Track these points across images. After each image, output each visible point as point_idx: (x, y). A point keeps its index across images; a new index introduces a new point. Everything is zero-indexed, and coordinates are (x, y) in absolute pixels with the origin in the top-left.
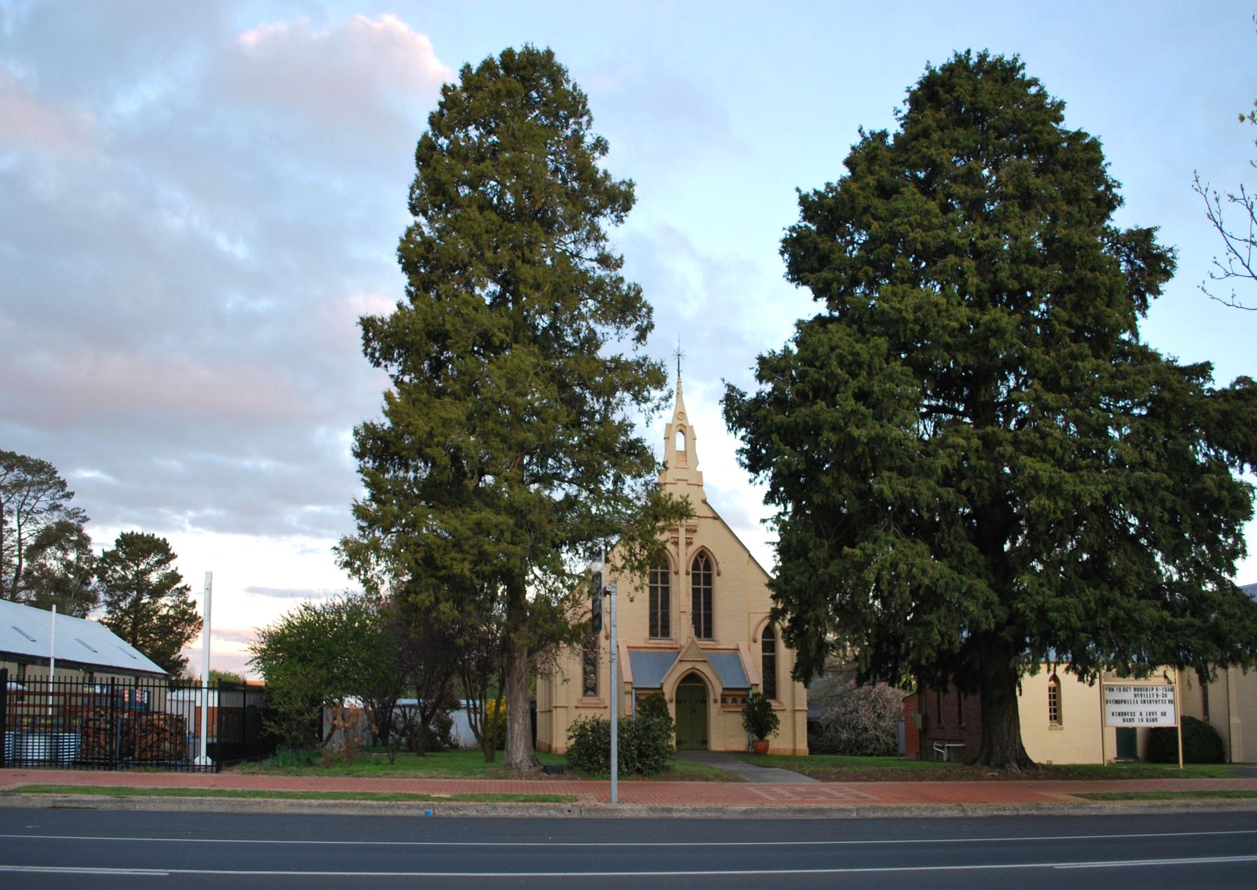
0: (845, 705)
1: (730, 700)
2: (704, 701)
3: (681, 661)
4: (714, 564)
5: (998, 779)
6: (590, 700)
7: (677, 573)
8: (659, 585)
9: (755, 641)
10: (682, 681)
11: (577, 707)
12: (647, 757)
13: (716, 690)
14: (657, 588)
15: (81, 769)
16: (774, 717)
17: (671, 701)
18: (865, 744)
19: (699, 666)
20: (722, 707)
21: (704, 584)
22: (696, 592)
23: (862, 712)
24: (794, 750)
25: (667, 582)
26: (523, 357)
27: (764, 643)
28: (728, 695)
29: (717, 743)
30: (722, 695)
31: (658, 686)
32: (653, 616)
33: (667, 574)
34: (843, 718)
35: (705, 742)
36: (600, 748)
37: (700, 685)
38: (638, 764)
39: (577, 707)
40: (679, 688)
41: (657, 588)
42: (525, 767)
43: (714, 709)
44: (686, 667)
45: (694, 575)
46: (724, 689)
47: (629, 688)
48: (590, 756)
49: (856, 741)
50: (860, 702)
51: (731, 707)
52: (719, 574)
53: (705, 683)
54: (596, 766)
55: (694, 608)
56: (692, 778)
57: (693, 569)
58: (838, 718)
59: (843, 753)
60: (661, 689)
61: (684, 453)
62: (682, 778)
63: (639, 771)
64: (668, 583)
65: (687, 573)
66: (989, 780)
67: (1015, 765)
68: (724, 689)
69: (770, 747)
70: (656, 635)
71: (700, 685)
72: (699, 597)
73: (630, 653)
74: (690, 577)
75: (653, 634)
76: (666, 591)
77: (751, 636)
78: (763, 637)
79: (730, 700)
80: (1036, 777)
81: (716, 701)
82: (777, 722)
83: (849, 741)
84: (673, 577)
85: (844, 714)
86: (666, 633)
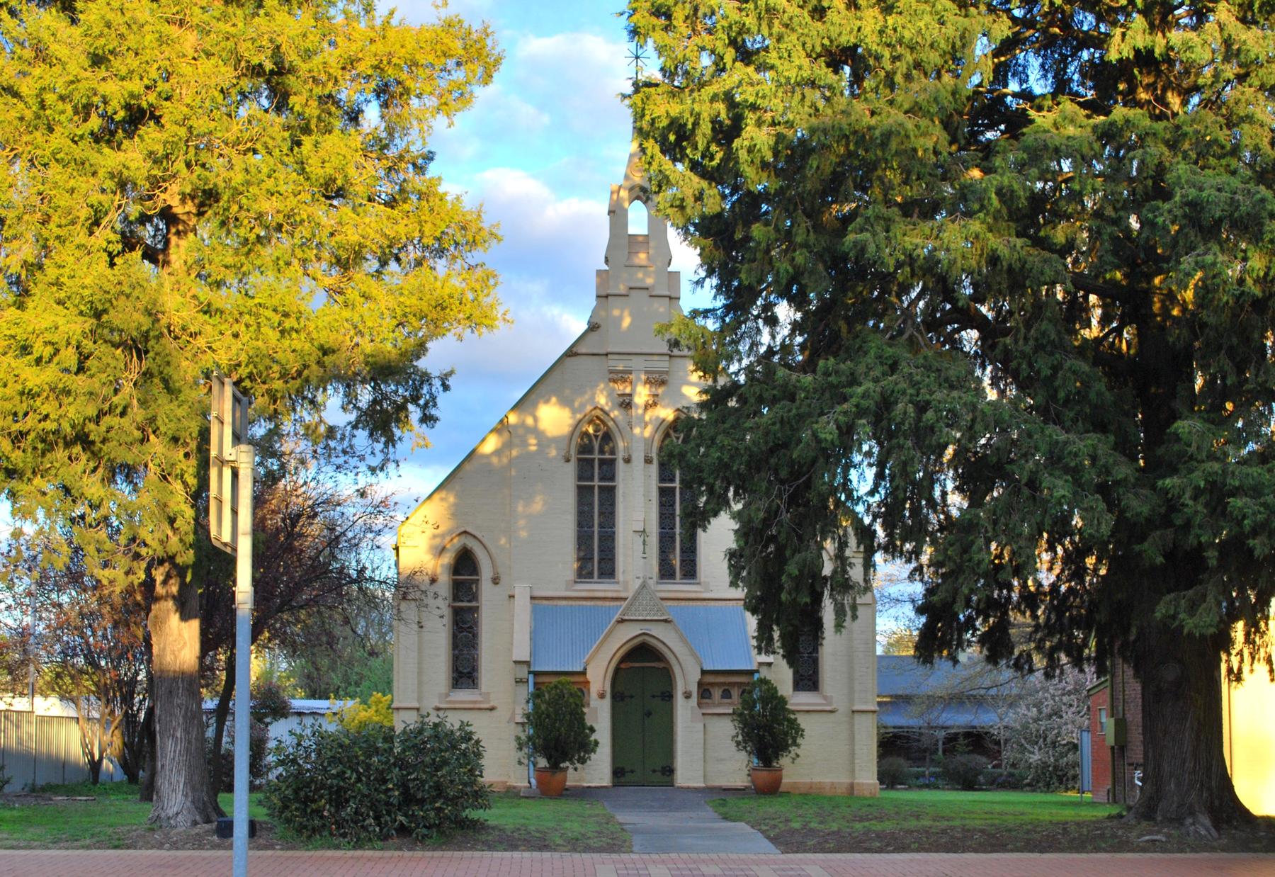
0: (1038, 705)
1: (717, 693)
2: (668, 696)
3: (621, 621)
5: (1164, 850)
6: (464, 696)
7: (628, 461)
10: (624, 659)
12: (421, 802)
13: (686, 679)
14: (601, 479)
16: (793, 725)
17: (602, 696)
18: (1071, 772)
19: (657, 631)
20: (700, 705)
21: (601, 479)
23: (1068, 715)
24: (852, 786)
25: (612, 478)
26: (756, 77)
28: (712, 684)
29: (687, 773)
30: (700, 684)
31: (579, 668)
32: (583, 540)
33: (612, 462)
34: (1033, 727)
35: (669, 771)
36: (323, 786)
37: (661, 665)
38: (401, 818)
40: (617, 671)
42: (183, 823)
43: (685, 712)
44: (628, 633)
46: (704, 672)
47: (523, 672)
48: (307, 801)
49: (1056, 768)
50: (1065, 699)
51: (720, 705)
53: (668, 662)
54: (317, 822)
55: (662, 525)
56: (541, 844)
58: (1025, 726)
59: (1033, 787)
60: (584, 673)
62: (510, 841)
63: (403, 831)
64: (612, 478)
65: (648, 461)
66: (1144, 850)
67: (1205, 820)
68: (704, 672)
69: (785, 780)
70: (590, 575)
71: (661, 665)
73: (535, 611)
75: (584, 573)
76: (609, 494)
79: (717, 693)
80: (1246, 847)
81: (688, 696)
82: (799, 731)
83: (1045, 765)
84: (621, 466)
85: (1036, 720)
86: (608, 571)
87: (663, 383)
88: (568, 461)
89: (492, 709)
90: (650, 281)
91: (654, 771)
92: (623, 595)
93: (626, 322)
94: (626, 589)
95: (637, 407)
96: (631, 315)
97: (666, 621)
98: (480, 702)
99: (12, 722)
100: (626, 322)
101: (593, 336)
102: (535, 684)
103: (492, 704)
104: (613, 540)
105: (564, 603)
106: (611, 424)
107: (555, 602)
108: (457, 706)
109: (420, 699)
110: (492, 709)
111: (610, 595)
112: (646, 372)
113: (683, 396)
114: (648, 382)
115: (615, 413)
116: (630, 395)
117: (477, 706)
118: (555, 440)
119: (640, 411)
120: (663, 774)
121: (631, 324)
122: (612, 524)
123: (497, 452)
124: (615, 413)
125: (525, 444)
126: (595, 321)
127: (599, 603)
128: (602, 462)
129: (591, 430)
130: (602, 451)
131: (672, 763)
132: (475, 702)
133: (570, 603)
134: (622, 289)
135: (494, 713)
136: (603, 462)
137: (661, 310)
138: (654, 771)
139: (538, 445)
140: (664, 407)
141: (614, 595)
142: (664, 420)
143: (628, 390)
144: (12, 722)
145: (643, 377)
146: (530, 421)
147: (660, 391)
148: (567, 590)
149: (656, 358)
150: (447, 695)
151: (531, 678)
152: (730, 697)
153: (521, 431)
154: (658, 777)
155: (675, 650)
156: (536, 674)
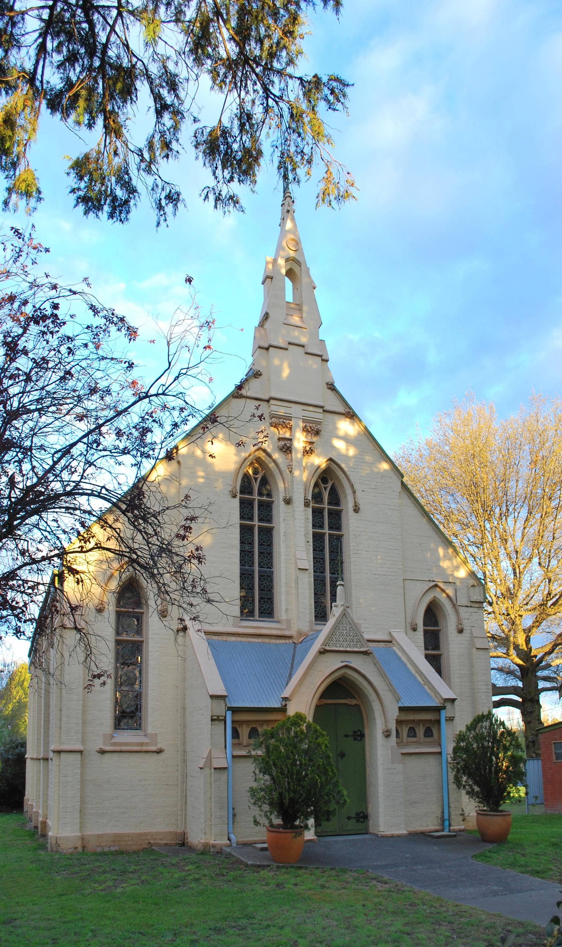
4: (349, 491)
7: (288, 502)
8: (256, 522)
9: (414, 629)
10: (324, 695)
11: (102, 752)
14: (323, 535)
15: (117, 838)
21: (260, 520)
22: (318, 539)
27: (425, 632)
28: (241, 723)
31: (277, 705)
39: (102, 752)
41: (323, 535)
45: (243, 502)
52: (356, 510)
57: (242, 492)
61: (16, 162)
64: (270, 521)
65: (307, 504)
70: (251, 613)
72: (251, 543)
74: (310, 510)
77: (409, 620)
78: (425, 625)
87: (317, 433)
88: (234, 496)
89: (159, 752)
90: (303, 340)
91: (349, 818)
92: (287, 633)
93: (286, 372)
94: (289, 628)
95: (297, 451)
96: (290, 366)
97: (366, 653)
98: (147, 744)
99: (25, 386)
100: (286, 372)
101: (254, 383)
102: (233, 722)
103: (159, 746)
104: (272, 580)
105: (233, 639)
106: (272, 465)
107: (224, 638)
108: (124, 748)
109: (83, 741)
110: (159, 752)
111: (275, 632)
112: (304, 421)
113: (333, 447)
114: (305, 429)
115: (276, 456)
116: (290, 440)
117: (144, 748)
118: (222, 475)
119: (299, 455)
120: (358, 821)
121: (290, 373)
122: (270, 564)
123: (168, 480)
124: (276, 456)
125: (193, 476)
126: (256, 368)
127: (267, 640)
128: (261, 504)
129: (251, 472)
130: (260, 494)
131: (367, 808)
132: (142, 744)
133: (239, 639)
134: (281, 342)
135: (162, 756)
136: (261, 504)
137: (315, 366)
138: (349, 818)
139: (206, 478)
140: (318, 455)
141: (279, 633)
142: (319, 467)
143: (288, 435)
144: (25, 386)
145: (301, 424)
146: (199, 453)
147: (314, 439)
148: (234, 626)
149: (311, 409)
150: (112, 737)
151: (229, 714)
152: (415, 736)
153: (191, 462)
154: (352, 824)
155: (378, 688)
156: (235, 710)
